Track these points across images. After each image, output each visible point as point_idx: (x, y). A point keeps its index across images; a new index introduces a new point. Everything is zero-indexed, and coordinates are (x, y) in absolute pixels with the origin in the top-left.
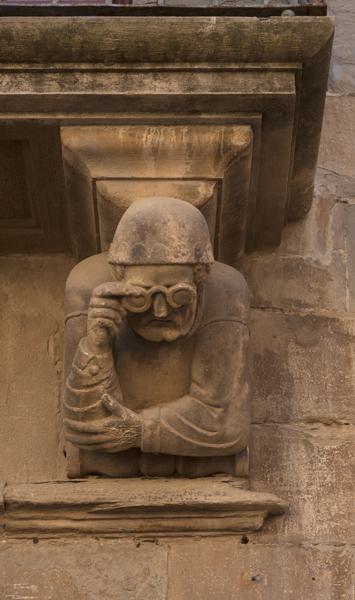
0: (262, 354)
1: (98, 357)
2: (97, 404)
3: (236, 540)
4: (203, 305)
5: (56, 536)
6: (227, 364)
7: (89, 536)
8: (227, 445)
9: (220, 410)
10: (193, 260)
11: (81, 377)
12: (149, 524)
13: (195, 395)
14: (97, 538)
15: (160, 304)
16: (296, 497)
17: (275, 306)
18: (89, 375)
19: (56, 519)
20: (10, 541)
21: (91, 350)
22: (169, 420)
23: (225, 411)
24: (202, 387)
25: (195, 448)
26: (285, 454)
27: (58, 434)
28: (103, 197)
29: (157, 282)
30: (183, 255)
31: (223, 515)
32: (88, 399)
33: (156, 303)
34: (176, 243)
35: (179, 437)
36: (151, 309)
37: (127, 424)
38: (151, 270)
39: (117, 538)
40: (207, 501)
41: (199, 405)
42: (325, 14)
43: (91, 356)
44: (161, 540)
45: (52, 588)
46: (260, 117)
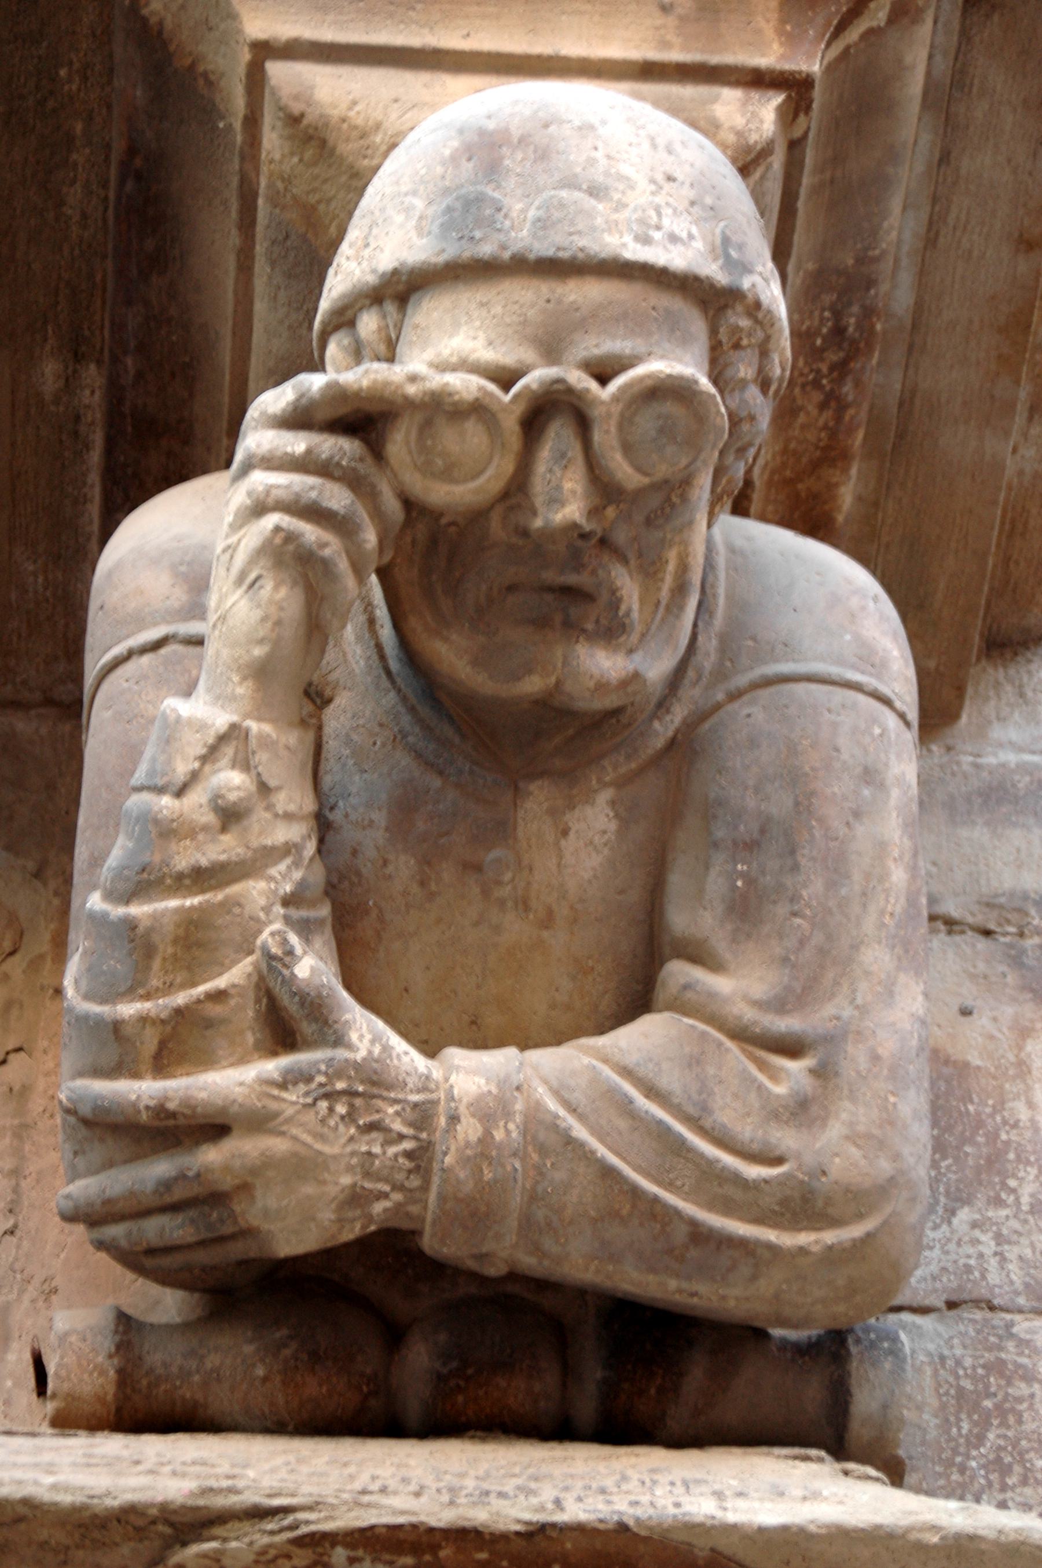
1: (254, 726)
2: (236, 974)
4: (719, 620)
8: (830, 1237)
10: (713, 270)
11: (169, 831)
13: (679, 1006)
15: (561, 456)
17: (955, 913)
18: (209, 818)
24: (715, 966)
28: (294, 120)
29: (551, 353)
30: (673, 238)
32: (195, 944)
33: (545, 453)
34: (641, 196)
35: (608, 1172)
36: (517, 490)
38: (526, 296)
40: (731, 1518)
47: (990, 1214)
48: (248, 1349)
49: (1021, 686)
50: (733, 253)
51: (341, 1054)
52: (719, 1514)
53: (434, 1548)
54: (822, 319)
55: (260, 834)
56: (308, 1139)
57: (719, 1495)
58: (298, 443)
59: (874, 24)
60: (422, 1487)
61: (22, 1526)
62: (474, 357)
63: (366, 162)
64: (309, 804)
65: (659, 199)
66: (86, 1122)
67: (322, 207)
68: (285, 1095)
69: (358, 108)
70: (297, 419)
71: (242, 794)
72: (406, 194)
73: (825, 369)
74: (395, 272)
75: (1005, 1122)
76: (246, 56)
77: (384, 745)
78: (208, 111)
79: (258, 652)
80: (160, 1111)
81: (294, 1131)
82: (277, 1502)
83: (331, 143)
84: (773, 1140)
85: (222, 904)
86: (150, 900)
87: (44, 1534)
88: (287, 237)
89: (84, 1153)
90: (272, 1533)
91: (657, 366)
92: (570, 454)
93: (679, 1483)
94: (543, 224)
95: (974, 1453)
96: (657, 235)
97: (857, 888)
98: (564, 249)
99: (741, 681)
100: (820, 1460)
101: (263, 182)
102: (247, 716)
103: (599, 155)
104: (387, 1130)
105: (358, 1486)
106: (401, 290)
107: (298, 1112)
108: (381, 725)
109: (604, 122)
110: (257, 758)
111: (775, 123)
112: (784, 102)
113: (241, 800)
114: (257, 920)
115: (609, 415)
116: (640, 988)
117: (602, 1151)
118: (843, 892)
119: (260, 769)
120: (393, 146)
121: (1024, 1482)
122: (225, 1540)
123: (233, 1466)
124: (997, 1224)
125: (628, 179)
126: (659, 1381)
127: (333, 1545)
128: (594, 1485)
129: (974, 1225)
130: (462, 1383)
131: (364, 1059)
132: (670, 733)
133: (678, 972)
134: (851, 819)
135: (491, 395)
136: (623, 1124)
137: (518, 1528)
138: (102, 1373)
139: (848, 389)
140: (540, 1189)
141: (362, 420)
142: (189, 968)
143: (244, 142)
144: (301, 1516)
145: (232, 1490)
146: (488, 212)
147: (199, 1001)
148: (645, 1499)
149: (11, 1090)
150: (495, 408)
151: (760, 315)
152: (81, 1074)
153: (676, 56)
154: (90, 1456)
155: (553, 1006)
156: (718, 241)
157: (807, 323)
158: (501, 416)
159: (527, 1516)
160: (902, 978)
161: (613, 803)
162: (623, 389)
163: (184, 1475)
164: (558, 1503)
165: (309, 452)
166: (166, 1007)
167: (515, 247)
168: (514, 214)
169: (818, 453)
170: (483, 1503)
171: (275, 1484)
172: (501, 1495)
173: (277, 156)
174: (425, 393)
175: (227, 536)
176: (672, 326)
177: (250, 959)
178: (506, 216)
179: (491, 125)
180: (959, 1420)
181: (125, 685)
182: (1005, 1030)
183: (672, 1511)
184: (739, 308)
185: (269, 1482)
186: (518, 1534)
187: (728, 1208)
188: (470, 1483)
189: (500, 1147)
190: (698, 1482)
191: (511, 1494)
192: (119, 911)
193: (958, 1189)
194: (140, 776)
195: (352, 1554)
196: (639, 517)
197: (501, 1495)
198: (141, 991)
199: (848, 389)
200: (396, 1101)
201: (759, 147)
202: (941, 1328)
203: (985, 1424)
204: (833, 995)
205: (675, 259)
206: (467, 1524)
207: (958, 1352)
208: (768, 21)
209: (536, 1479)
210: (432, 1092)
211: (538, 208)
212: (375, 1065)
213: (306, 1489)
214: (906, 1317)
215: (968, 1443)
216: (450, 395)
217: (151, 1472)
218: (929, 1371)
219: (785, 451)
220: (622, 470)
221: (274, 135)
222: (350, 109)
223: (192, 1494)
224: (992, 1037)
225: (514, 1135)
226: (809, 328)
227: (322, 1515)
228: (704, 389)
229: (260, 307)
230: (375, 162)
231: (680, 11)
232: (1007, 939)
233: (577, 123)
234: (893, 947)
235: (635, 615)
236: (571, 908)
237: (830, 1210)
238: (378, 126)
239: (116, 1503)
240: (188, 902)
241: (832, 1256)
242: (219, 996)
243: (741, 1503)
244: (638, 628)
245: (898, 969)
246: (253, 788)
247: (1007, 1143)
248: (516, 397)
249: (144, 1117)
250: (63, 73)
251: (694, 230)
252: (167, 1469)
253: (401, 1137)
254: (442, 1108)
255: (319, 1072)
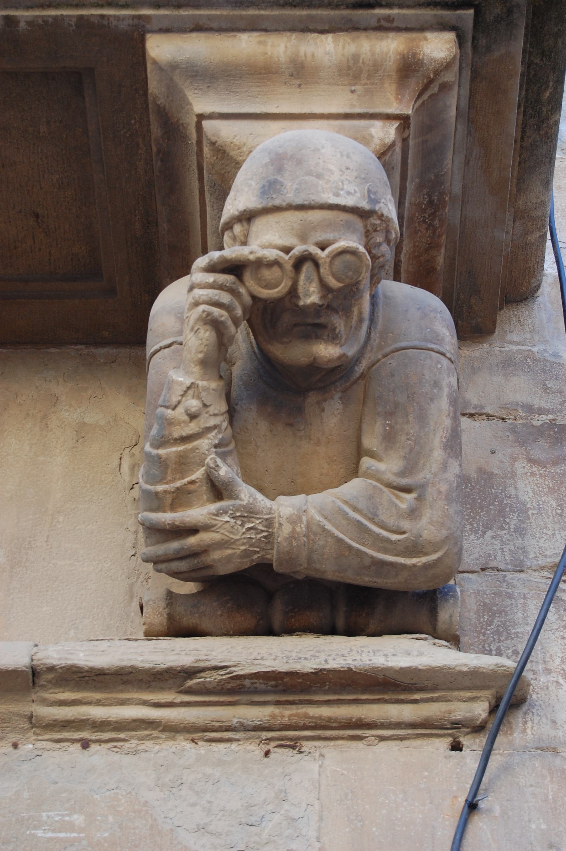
0: (474, 475)
2: (199, 474)
3: (442, 745)
4: (380, 327)
5: (122, 736)
6: (422, 418)
7: (180, 737)
8: (424, 560)
9: (410, 497)
10: (365, 205)
11: (170, 423)
12: (287, 713)
13: (367, 475)
14: (193, 741)
16: (543, 679)
17: (491, 413)
18: (186, 418)
19: (123, 703)
20: (39, 744)
21: (188, 373)
22: (321, 511)
23: (419, 499)
24: (380, 460)
25: (367, 562)
26: (520, 615)
27: (131, 586)
28: (213, 144)
30: (349, 193)
31: (417, 696)
32: (183, 464)
33: (302, 277)
34: (336, 177)
35: (340, 540)
36: (293, 292)
37: (249, 513)
39: (230, 740)
40: (390, 664)
41: (375, 487)
42: (461, 750)
43: (188, 383)
44: (307, 745)
45: (111, 819)
46: (471, 12)
47: (499, 533)
48: (215, 604)
49: (519, 318)
50: (372, 196)
51: (238, 502)
52: (385, 663)
53: (282, 679)
54: (424, 198)
55: (204, 423)
56: (228, 534)
57: (386, 655)
58: (210, 278)
59: (433, 92)
60: (276, 657)
61: (132, 675)
62: (274, 243)
63: (241, 158)
64: (224, 407)
65: (343, 178)
66: (148, 528)
67: (226, 174)
68: (218, 518)
69: (236, 138)
70: (211, 269)
71: (197, 409)
72: (249, 180)
73: (427, 216)
74: (245, 211)
75: (506, 496)
76: (195, 119)
77: (254, 380)
78: (185, 138)
79: (201, 356)
80: (173, 525)
81: (222, 531)
82: (223, 664)
83: (227, 151)
84: (402, 526)
85: (191, 449)
86: (166, 448)
87: (140, 677)
88: (215, 185)
89: (149, 538)
90: (222, 675)
91: (342, 244)
92: (312, 278)
93: (371, 651)
94: (298, 191)
95: (489, 628)
96: (342, 193)
97: (432, 428)
98: (306, 200)
99: (388, 350)
100: (426, 639)
101: (205, 165)
102: (197, 379)
103: (320, 161)
104: (257, 529)
105: (253, 657)
106: (248, 217)
107: (223, 524)
108: (253, 373)
109: (323, 147)
110: (202, 394)
111: (395, 134)
112: (398, 126)
113: (196, 411)
114: (205, 454)
115: (325, 262)
116: (354, 466)
117: (337, 533)
118: (427, 429)
119: (203, 399)
120: (251, 152)
121: (507, 639)
122: (206, 678)
123: (208, 650)
124: (501, 537)
125: (331, 170)
126: (366, 611)
127: (245, 679)
128: (340, 654)
129: (493, 537)
130: (293, 614)
131: (247, 504)
132: (361, 371)
133: (366, 462)
134: (429, 402)
135: (281, 257)
136: (345, 522)
137: (312, 671)
138: (162, 615)
139: (436, 223)
140: (314, 548)
141: (236, 268)
142: (181, 472)
143: (197, 150)
144: (232, 669)
145: (207, 660)
146: (278, 187)
147: (185, 485)
148: (358, 658)
149: (135, 499)
150: (282, 262)
151: (384, 219)
152: (146, 510)
153: (357, 110)
154: (156, 648)
155: (321, 475)
156: (366, 192)
157: (418, 200)
158: (285, 265)
159: (315, 667)
160: (450, 460)
161: (341, 398)
162: (330, 253)
163: (190, 655)
164: (326, 661)
165: (214, 281)
166: (173, 487)
167: (288, 201)
168: (288, 187)
169: (427, 246)
170: (299, 662)
171: (222, 657)
172: (306, 659)
173: (208, 157)
174: (256, 258)
175: (187, 313)
176: (348, 226)
177: (204, 468)
178: (285, 188)
179: (280, 151)
180: (484, 615)
181: (160, 360)
182: (507, 459)
183: (368, 662)
184: (375, 217)
185: (220, 657)
186: (312, 673)
187: (385, 551)
188: (294, 654)
189: (298, 533)
190: (378, 651)
191: (309, 658)
192: (154, 452)
193: (487, 524)
194: (160, 402)
195: (252, 681)
196: (340, 299)
197: (306, 659)
198: (165, 481)
199: (436, 223)
200: (259, 518)
201: (389, 144)
202: (479, 579)
203: (494, 615)
204: (423, 469)
205: (349, 201)
206: (292, 670)
207: (485, 588)
208: (392, 95)
209: (319, 652)
210: (273, 514)
211: (297, 184)
212: (251, 506)
213: (234, 659)
214: (466, 575)
215: (487, 624)
216: (266, 258)
217: (178, 654)
218: (473, 596)
219: (414, 246)
220: (333, 283)
221: (207, 149)
222: (234, 138)
223: (193, 662)
224: (502, 462)
225: (304, 529)
226: (419, 202)
227: (240, 668)
228: (361, 251)
229: (208, 209)
230: (244, 158)
231: (359, 93)
232: (510, 422)
233: (313, 148)
234: (446, 449)
235: (342, 332)
236: (327, 438)
237: (424, 550)
238: (245, 144)
239: (165, 666)
240: (179, 449)
241: (426, 567)
242: (192, 482)
243: (394, 658)
244: (344, 337)
245: (448, 457)
246: (201, 405)
247: (506, 504)
248: (290, 257)
249: (168, 527)
250: (133, 122)
251: (357, 189)
252: (184, 652)
253: (263, 531)
254: (276, 520)
255: (230, 509)
